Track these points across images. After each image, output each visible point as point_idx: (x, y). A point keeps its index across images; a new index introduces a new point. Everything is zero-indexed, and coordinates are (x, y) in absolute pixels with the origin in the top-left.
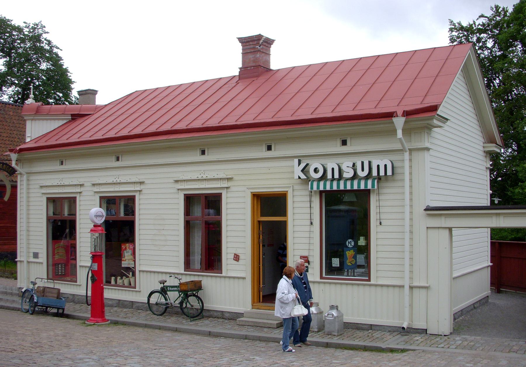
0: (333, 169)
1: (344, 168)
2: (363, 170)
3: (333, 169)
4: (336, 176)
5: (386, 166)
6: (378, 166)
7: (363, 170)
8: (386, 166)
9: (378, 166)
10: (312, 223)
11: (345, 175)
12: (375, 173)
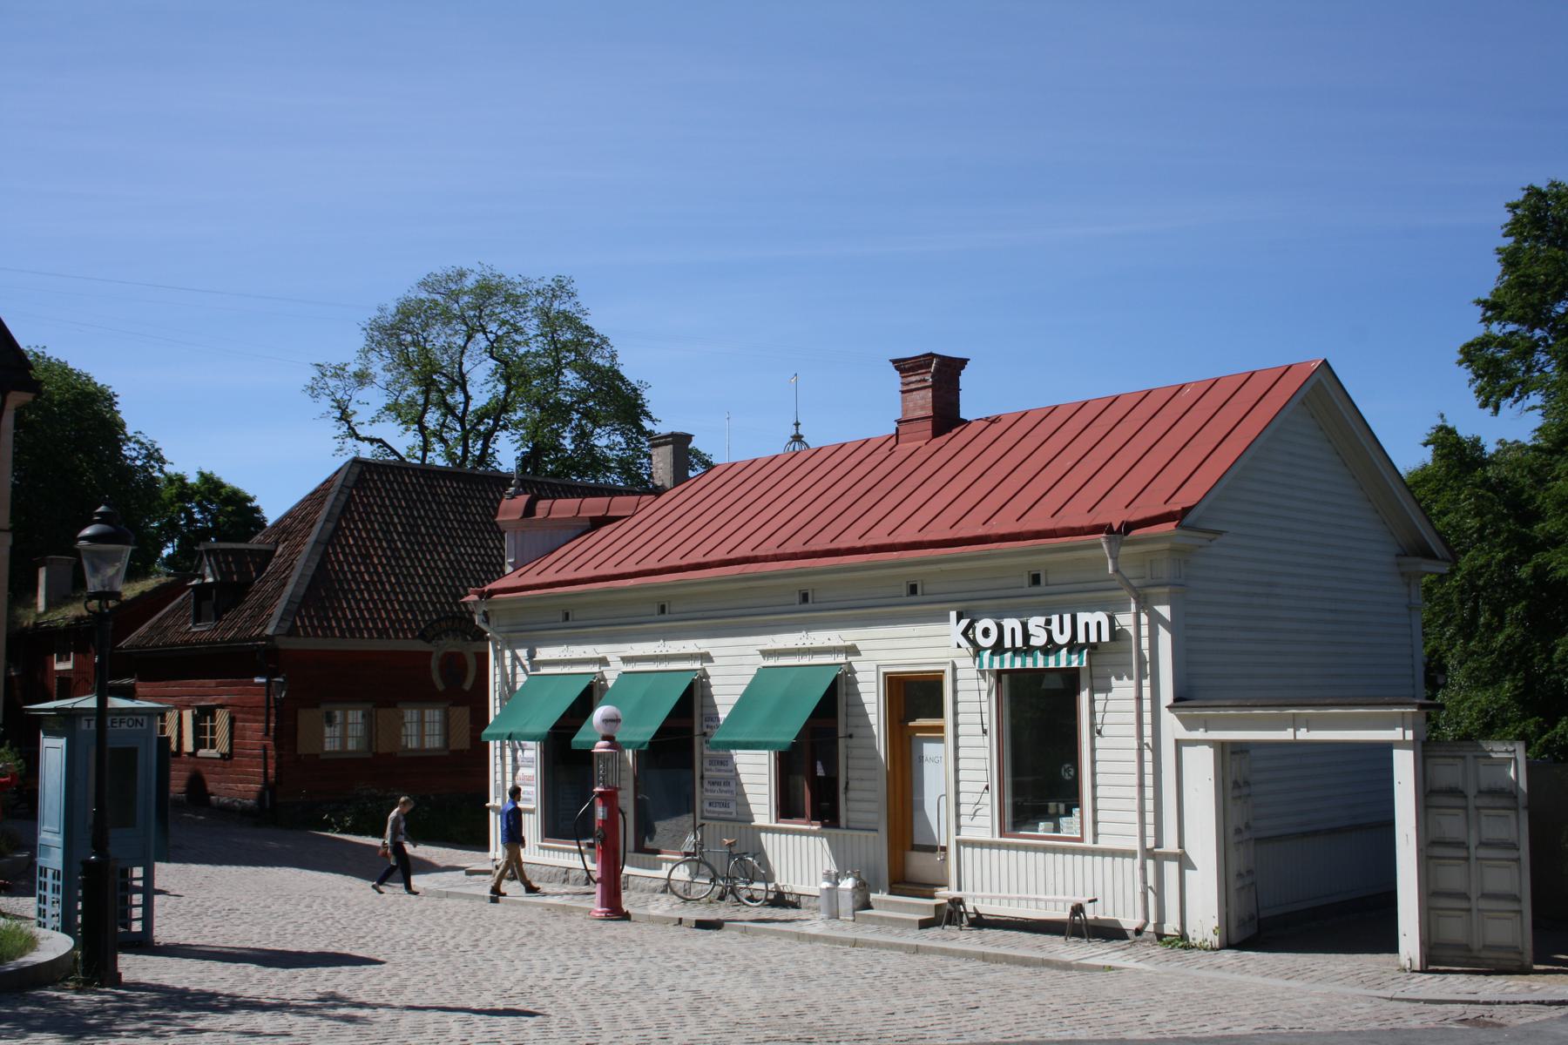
0: (1013, 630)
1: (1032, 629)
2: (1062, 632)
3: (1013, 630)
4: (1019, 643)
5: (1099, 624)
6: (1087, 625)
7: (1062, 632)
8: (1099, 624)
9: (1087, 625)
10: (985, 732)
11: (1034, 642)
12: (1081, 639)
